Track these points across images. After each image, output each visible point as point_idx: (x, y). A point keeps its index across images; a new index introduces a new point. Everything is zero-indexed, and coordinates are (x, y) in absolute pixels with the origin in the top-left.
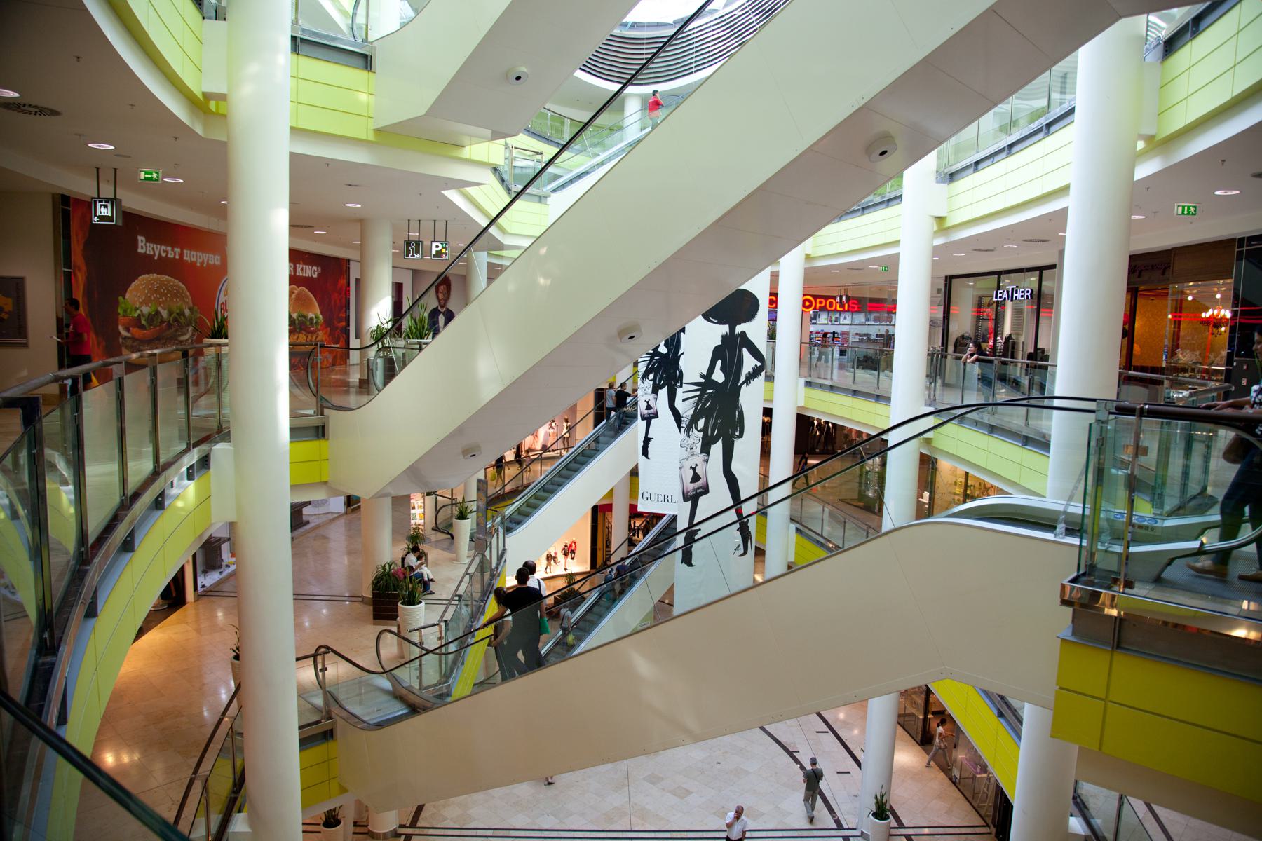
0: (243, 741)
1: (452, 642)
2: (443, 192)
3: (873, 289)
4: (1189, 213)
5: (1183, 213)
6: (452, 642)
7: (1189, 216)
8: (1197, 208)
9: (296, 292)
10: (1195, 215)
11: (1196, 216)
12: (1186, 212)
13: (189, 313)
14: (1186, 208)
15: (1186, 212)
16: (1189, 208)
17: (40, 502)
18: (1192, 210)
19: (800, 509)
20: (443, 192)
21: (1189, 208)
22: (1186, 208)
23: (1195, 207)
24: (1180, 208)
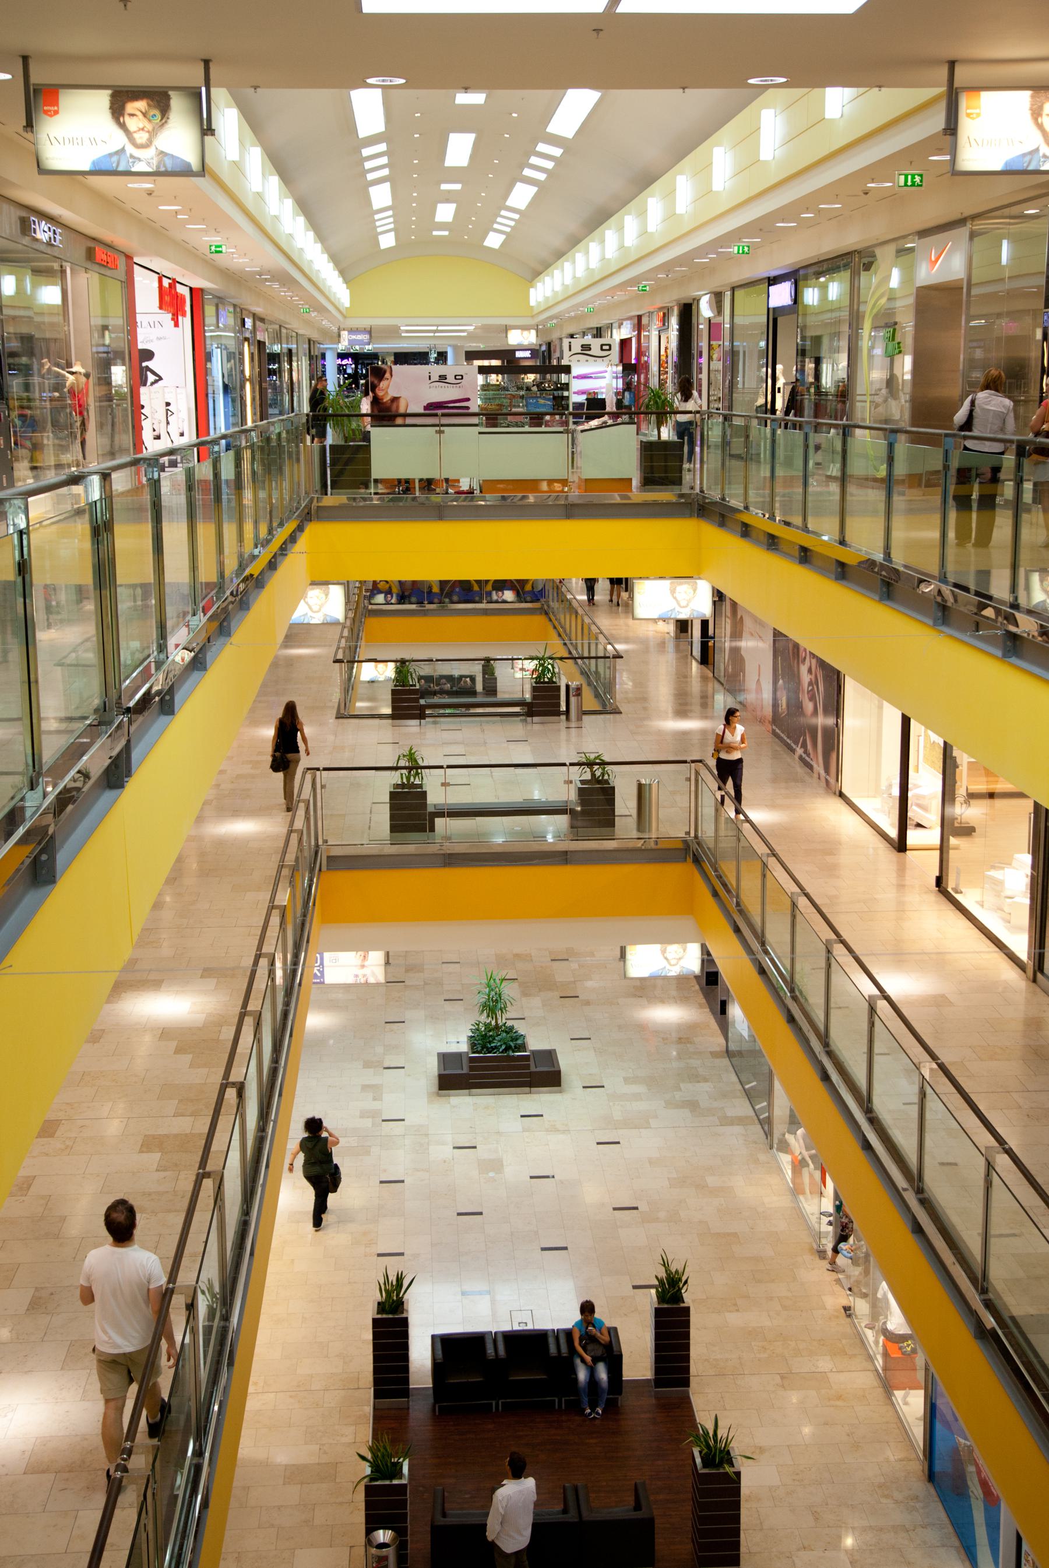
0: (687, 682)
1: (805, 519)
2: (730, 778)
3: (276, 411)
4: (913, 185)
5: (906, 185)
6: (805, 519)
7: (913, 188)
8: (924, 177)
9: (1016, 899)
10: (921, 186)
11: (923, 188)
12: (909, 183)
13: (114, 369)
14: (910, 177)
15: (909, 183)
16: (913, 178)
17: (951, 535)
18: (917, 179)
19: (838, 446)
20: (730, 778)
21: (913, 178)
22: (910, 177)
23: (921, 176)
24: (902, 178)
